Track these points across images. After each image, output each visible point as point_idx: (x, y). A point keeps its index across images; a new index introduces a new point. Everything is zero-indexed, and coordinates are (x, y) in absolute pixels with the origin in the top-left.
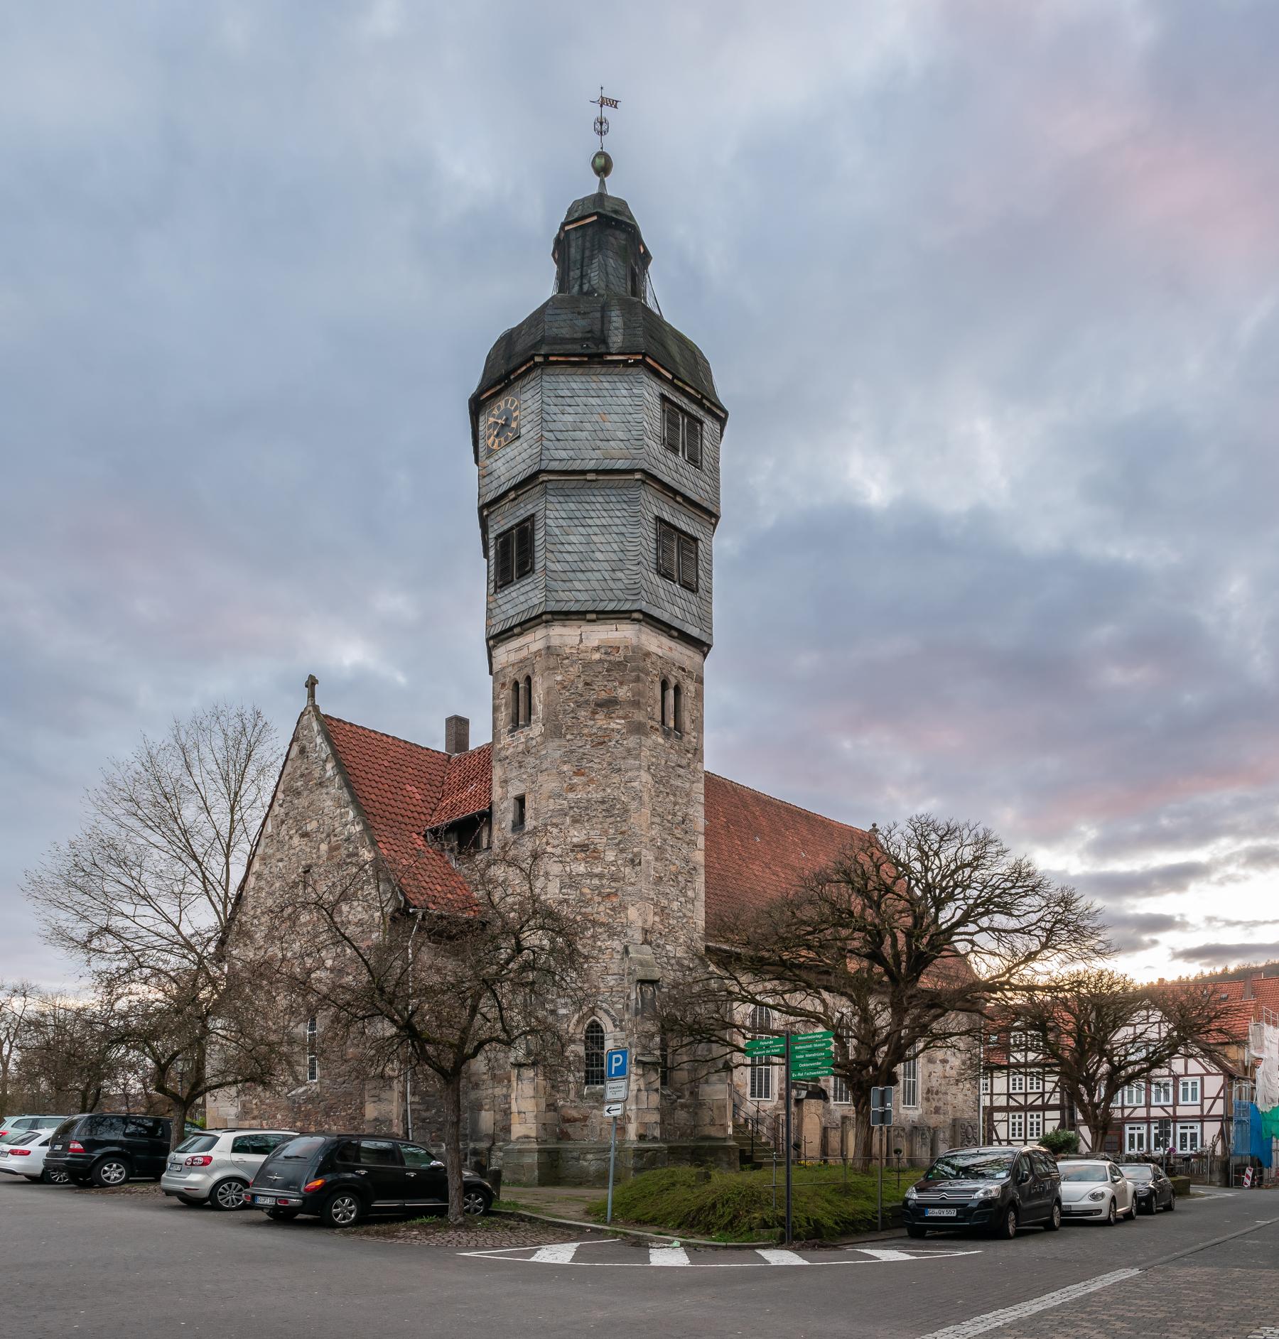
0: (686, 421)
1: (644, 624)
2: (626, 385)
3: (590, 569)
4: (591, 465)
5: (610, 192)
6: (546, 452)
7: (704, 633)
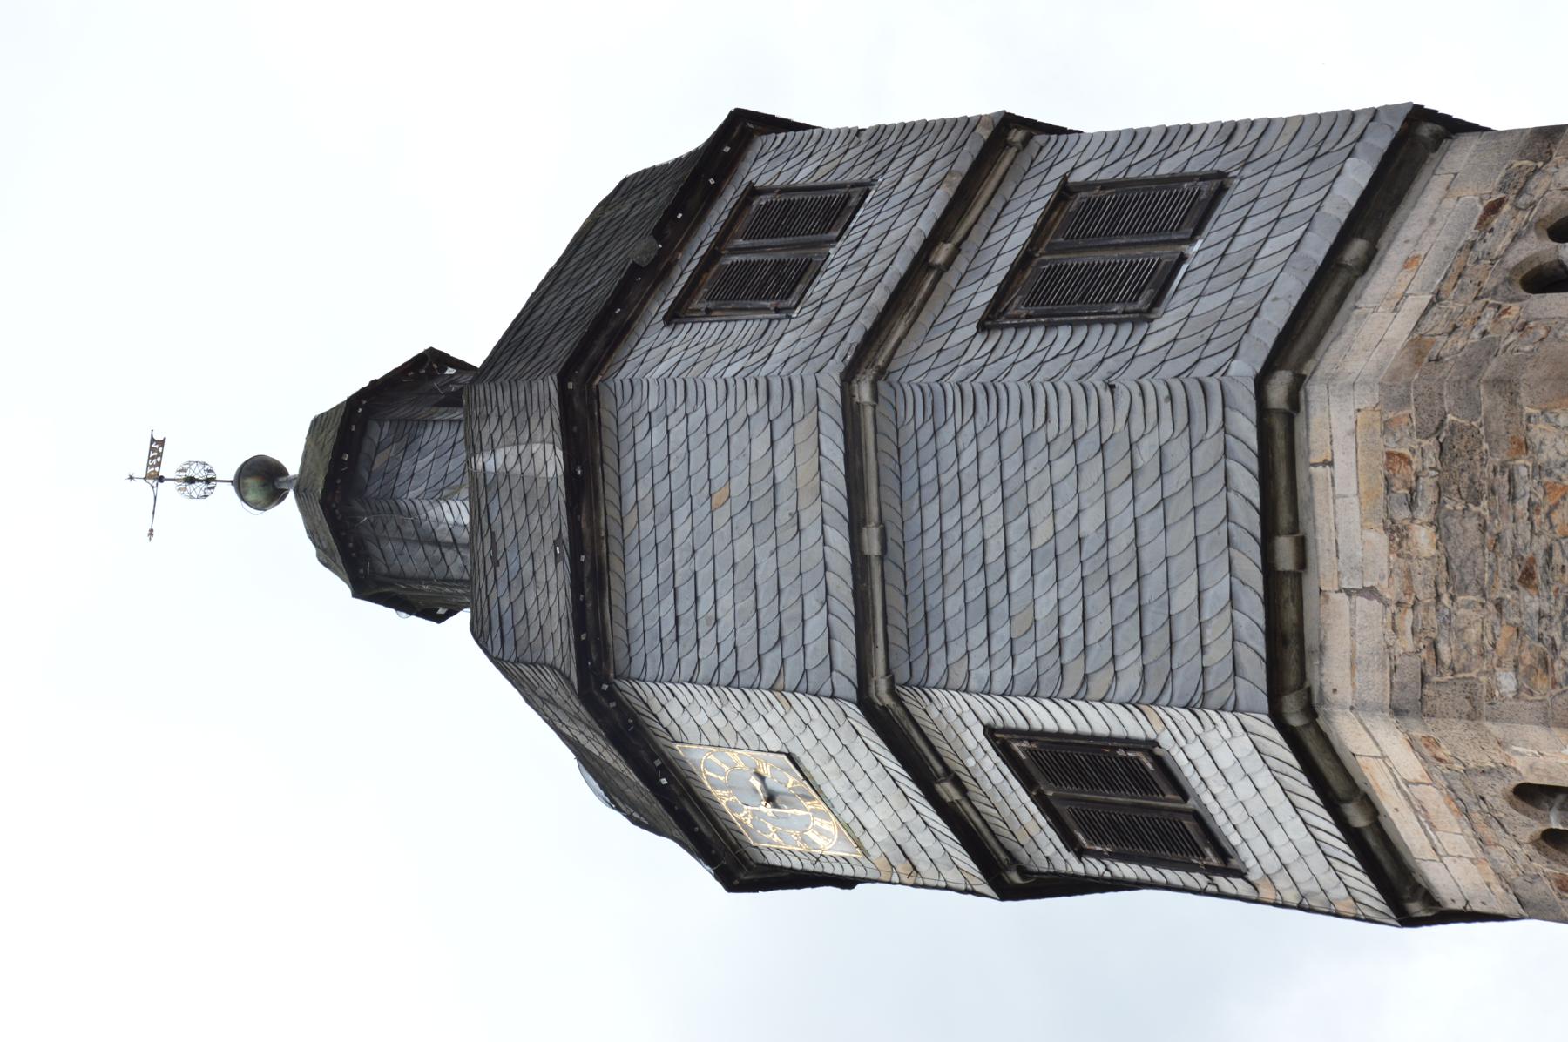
0: (740, 242)
1: (1310, 365)
2: (641, 430)
3: (1131, 553)
4: (839, 541)
5: (232, 478)
6: (812, 676)
7: (1368, 139)
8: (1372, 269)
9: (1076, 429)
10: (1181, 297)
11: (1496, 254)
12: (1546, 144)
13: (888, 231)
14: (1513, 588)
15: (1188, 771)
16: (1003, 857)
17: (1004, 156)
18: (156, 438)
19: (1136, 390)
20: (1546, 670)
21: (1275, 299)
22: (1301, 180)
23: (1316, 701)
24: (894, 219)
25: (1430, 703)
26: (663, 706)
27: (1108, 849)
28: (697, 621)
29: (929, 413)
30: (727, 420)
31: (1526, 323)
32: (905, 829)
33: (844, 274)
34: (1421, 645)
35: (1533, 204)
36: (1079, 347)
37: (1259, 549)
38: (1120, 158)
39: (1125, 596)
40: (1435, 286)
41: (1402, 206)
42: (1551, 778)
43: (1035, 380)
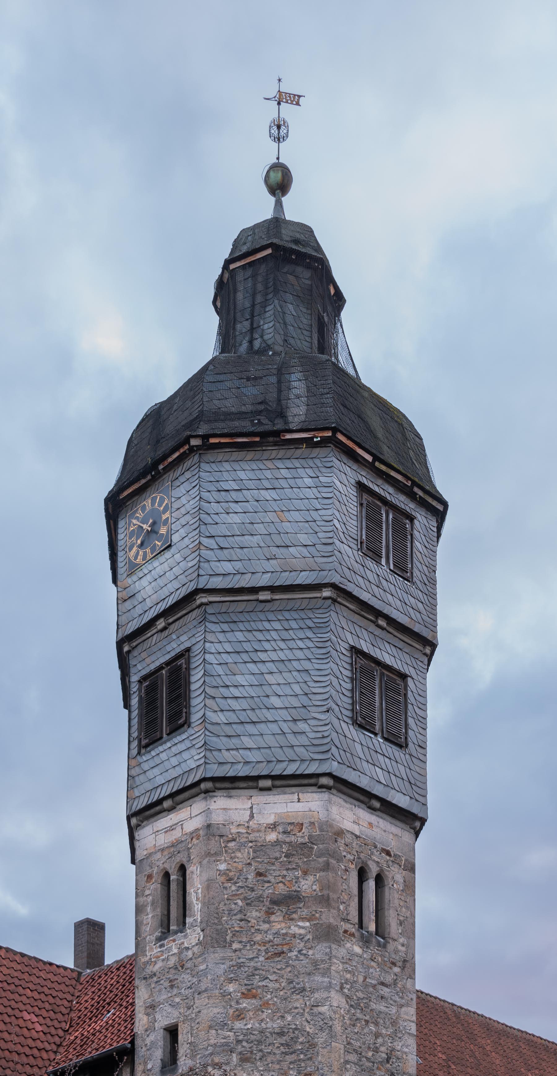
0: (391, 516)
2: (309, 471)
3: (264, 719)
4: (264, 581)
8: (369, 810)
9: (311, 695)
10: (362, 736)
11: (372, 857)
12: (409, 868)
13: (392, 595)
14: (256, 869)
15: (179, 738)
16: (134, 644)
17: (419, 645)
18: (301, 99)
19: (327, 722)
20: (227, 880)
21: (359, 776)
22: (403, 779)
23: (211, 794)
24: (398, 597)
25: (213, 838)
26: (188, 479)
27: (143, 695)
28: (227, 502)
29: (318, 625)
30: (315, 521)
31: (348, 871)
32: (143, 600)
33: (375, 576)
34: (234, 835)
35: (389, 867)
36: (343, 694)
37: (267, 774)
38: (416, 700)
39: (246, 716)
40: (362, 836)
41: (391, 818)
42: (189, 879)
43: (331, 676)
